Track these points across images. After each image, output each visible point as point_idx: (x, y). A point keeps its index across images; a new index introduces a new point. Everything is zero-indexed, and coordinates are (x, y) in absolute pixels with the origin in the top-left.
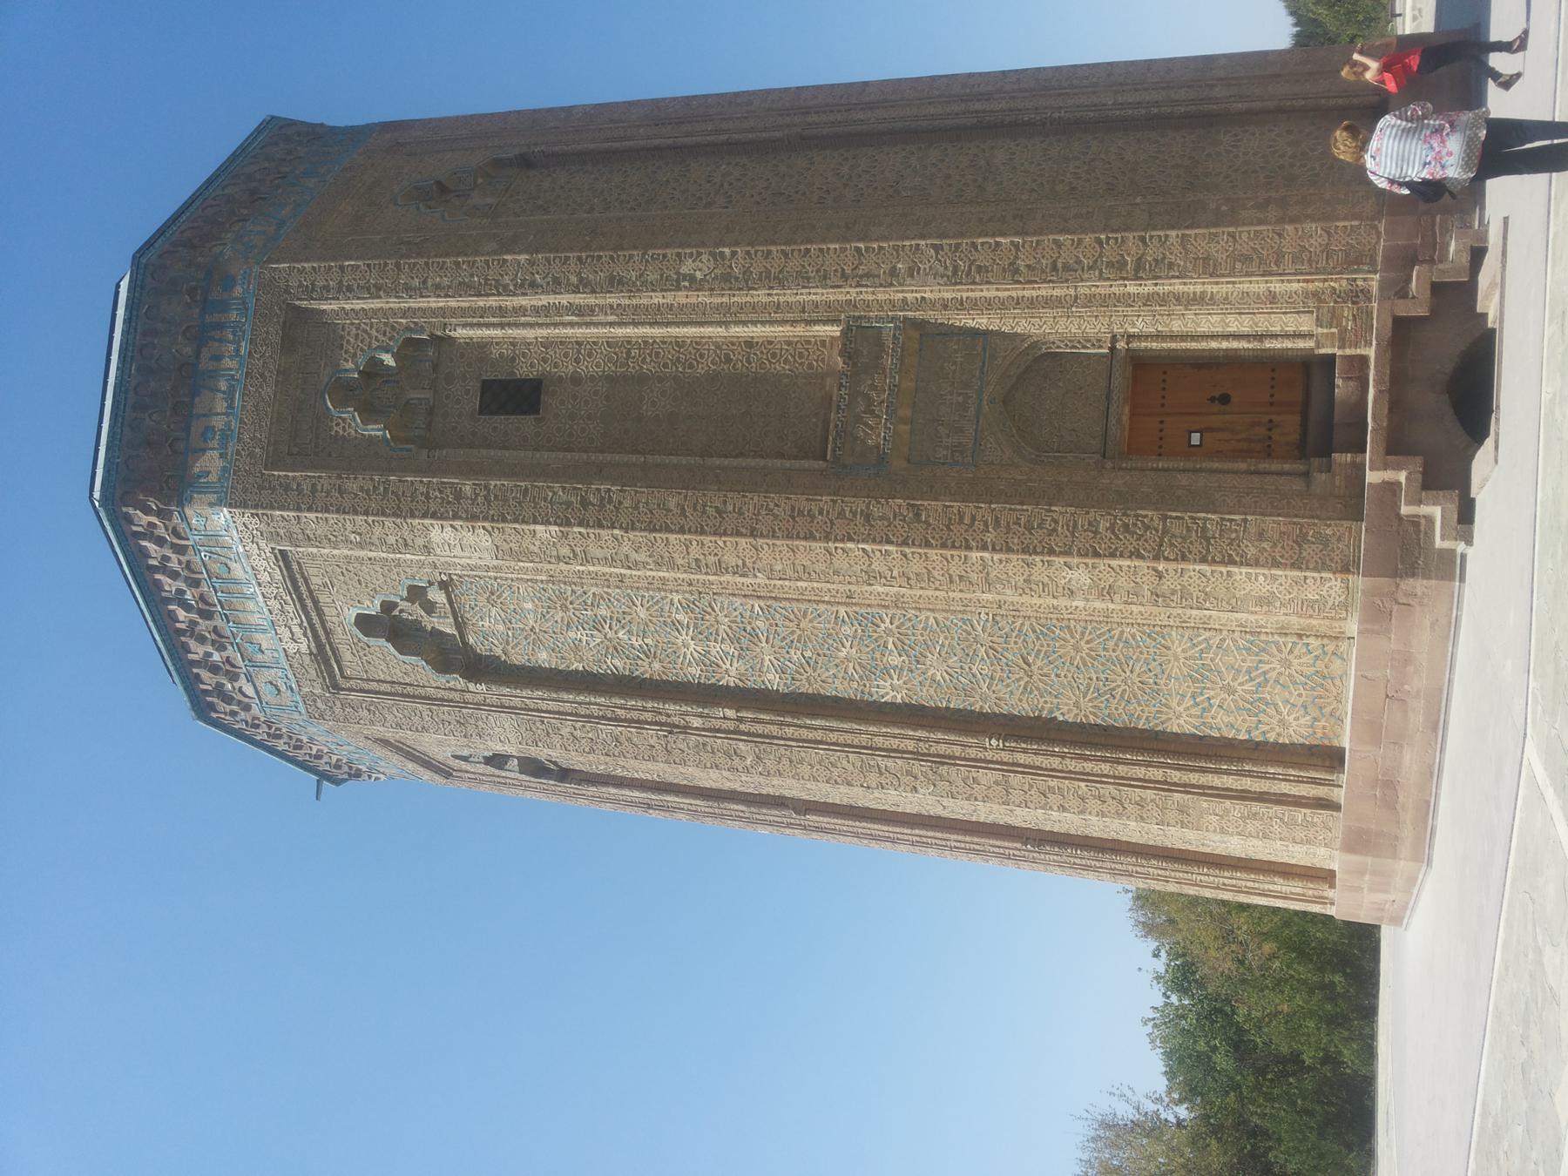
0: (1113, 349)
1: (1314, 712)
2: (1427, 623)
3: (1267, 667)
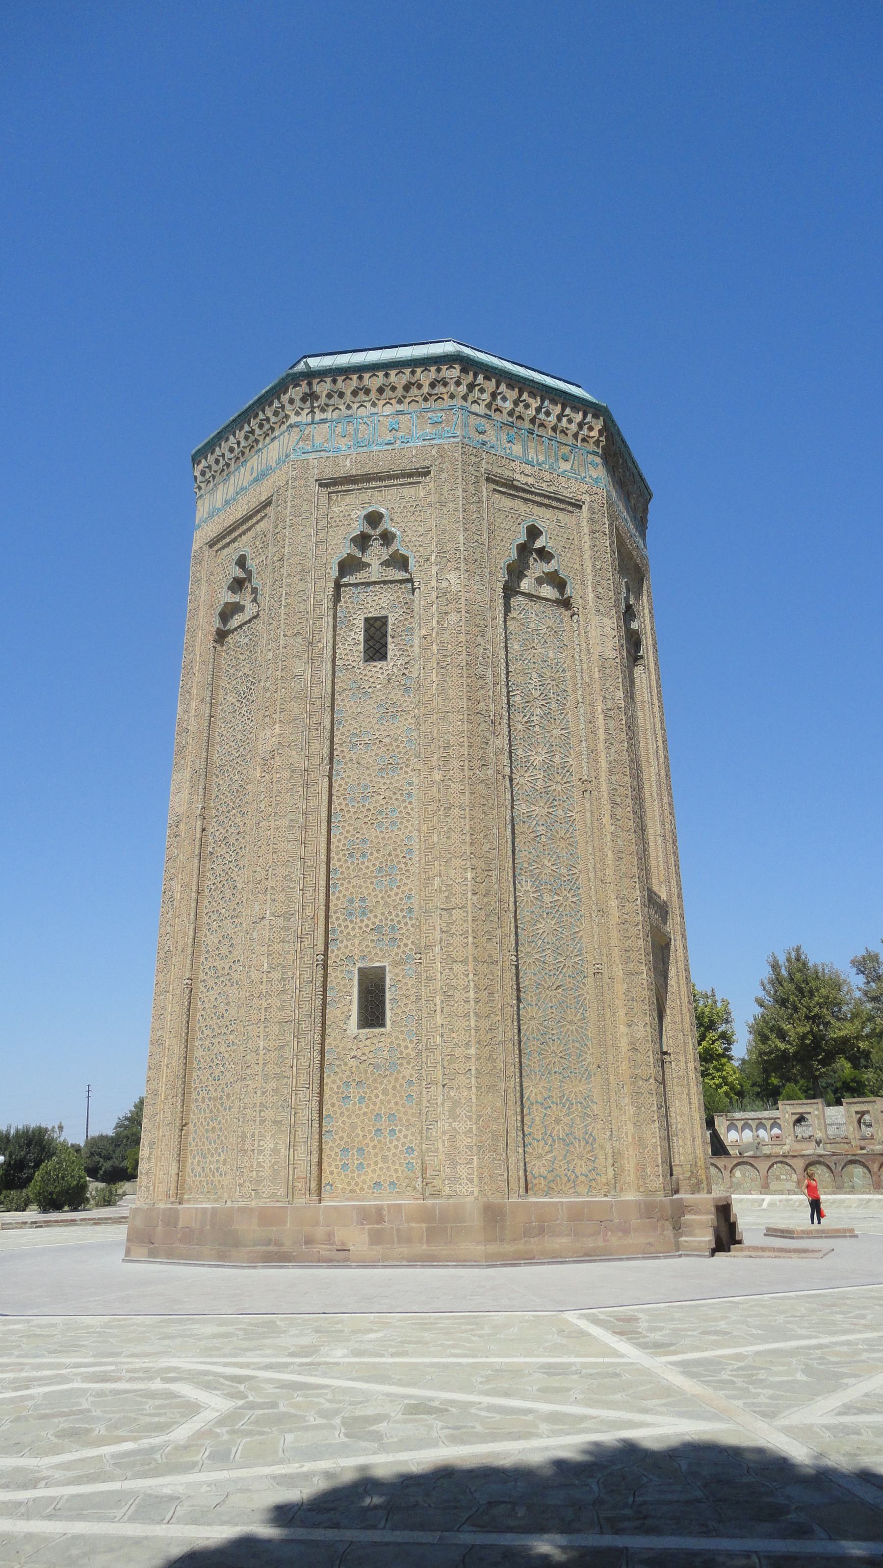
2: (651, 1240)
3: (577, 1145)
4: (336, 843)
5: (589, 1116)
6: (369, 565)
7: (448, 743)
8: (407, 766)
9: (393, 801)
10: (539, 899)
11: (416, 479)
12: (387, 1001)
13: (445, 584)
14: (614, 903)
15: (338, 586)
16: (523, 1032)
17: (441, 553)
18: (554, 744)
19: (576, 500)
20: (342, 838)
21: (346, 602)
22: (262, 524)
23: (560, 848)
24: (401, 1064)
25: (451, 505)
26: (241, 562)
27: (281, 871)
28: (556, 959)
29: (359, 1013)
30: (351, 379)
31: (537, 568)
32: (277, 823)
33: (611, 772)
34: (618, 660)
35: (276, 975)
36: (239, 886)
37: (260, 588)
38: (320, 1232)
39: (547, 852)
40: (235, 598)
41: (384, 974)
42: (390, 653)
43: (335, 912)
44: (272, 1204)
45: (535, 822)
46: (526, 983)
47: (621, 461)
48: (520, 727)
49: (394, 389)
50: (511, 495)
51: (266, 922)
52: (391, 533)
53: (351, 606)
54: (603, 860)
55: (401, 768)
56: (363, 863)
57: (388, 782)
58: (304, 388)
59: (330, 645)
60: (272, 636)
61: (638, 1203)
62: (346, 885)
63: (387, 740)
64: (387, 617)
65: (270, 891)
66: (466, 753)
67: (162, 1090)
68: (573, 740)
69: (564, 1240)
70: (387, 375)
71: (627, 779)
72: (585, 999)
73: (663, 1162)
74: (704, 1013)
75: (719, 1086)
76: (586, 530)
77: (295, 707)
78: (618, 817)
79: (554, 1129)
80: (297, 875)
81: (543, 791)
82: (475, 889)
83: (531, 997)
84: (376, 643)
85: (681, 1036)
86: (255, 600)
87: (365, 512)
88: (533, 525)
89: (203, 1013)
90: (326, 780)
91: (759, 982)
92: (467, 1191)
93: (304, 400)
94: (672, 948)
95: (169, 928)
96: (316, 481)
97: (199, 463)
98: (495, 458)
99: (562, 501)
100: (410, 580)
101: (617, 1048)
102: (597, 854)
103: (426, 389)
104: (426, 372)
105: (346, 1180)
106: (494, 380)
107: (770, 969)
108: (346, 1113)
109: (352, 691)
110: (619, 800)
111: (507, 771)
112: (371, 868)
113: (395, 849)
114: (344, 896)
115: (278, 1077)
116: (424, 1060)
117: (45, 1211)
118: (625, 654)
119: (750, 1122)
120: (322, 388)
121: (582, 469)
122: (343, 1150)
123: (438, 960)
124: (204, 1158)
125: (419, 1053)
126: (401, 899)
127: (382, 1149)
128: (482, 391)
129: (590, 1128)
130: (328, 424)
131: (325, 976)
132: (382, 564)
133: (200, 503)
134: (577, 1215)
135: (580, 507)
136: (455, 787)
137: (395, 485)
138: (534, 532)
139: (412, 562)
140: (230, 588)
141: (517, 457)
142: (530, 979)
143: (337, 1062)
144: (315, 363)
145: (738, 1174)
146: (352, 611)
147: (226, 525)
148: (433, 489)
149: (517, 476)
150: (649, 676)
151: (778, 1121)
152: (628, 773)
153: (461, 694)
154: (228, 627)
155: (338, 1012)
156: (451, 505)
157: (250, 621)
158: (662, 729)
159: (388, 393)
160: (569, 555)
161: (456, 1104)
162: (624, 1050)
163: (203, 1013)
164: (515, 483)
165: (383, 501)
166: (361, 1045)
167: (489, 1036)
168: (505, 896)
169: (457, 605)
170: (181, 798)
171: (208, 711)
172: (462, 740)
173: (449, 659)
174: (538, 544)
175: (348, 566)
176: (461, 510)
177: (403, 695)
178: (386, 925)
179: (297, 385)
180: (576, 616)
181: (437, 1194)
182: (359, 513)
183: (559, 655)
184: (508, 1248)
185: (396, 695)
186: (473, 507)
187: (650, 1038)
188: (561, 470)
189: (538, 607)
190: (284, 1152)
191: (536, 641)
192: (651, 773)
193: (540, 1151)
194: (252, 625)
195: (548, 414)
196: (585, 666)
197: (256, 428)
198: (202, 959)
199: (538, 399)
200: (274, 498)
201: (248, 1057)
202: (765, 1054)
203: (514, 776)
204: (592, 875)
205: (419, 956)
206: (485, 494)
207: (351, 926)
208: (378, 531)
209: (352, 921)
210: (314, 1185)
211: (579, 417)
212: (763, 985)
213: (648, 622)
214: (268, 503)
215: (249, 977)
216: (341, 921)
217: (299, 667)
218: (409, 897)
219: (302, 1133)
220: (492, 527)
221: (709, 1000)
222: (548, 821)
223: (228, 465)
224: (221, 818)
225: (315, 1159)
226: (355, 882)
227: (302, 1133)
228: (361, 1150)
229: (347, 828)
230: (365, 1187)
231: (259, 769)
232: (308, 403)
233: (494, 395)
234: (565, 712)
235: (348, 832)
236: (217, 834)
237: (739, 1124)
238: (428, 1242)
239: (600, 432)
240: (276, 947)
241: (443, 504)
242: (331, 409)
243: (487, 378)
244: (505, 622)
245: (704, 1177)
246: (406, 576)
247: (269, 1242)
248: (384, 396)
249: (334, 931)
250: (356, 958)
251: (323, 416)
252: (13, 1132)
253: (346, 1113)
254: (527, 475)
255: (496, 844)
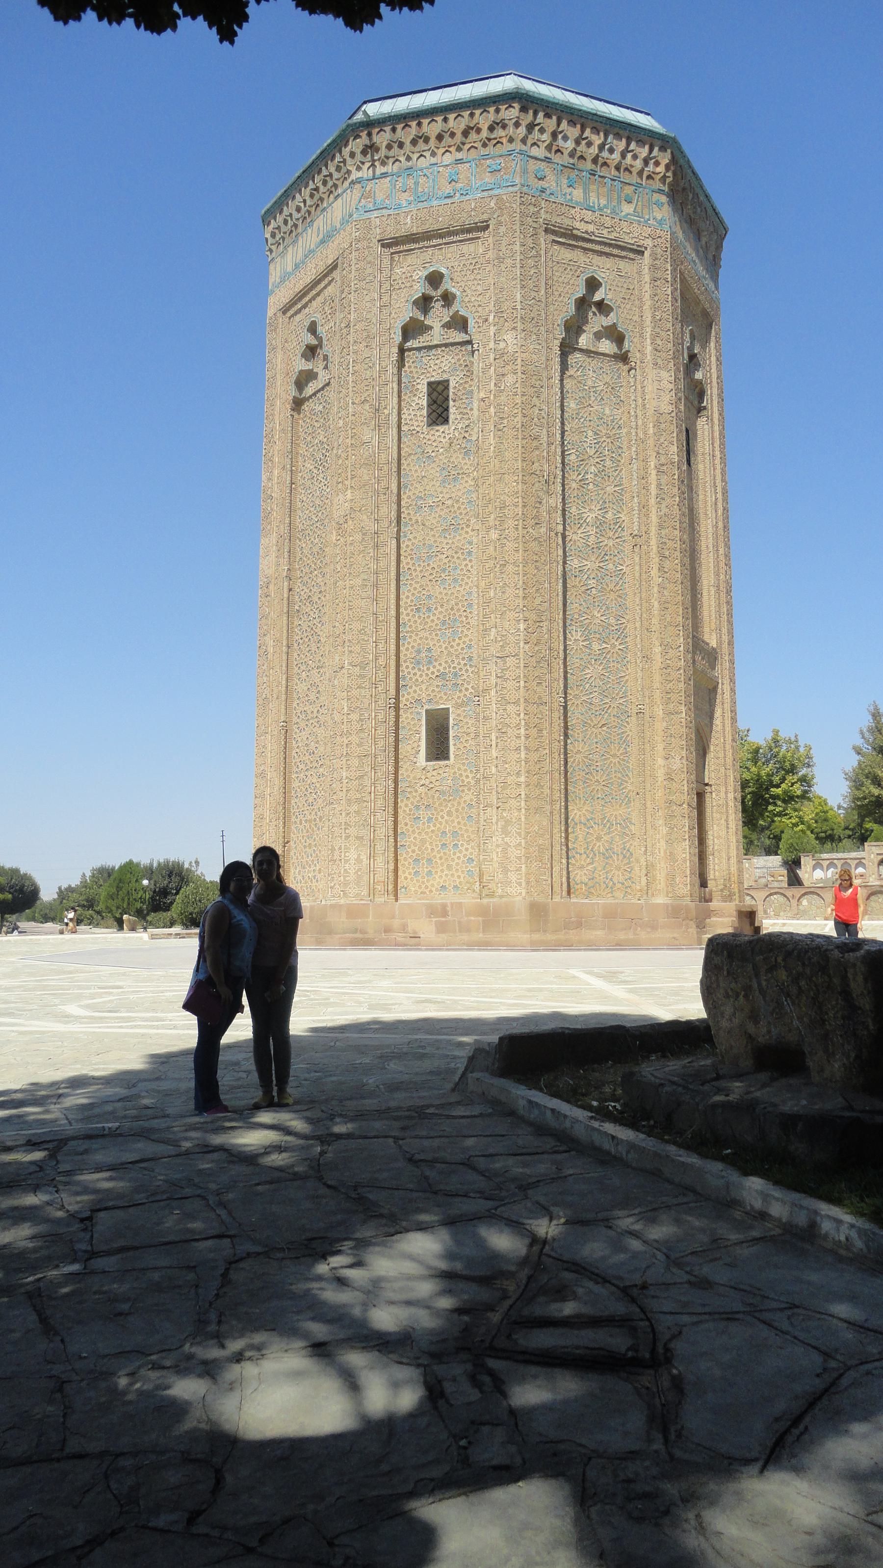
0: (707, 785)
1: (590, 884)
2: (675, 935)
4: (405, 600)
5: (627, 835)
6: (431, 328)
7: (504, 503)
8: (468, 526)
9: (455, 559)
11: (475, 235)
12: (451, 738)
13: (502, 345)
14: (658, 650)
15: (402, 351)
16: (569, 764)
17: (499, 312)
18: (607, 501)
19: (638, 246)
20: (410, 595)
21: (410, 367)
22: (329, 288)
23: (609, 600)
24: (463, 791)
25: (509, 261)
26: (313, 329)
27: (357, 626)
29: (427, 748)
30: (410, 126)
31: (596, 322)
32: (351, 582)
33: (661, 527)
34: (674, 414)
35: (355, 717)
36: (323, 640)
37: (330, 355)
38: (396, 923)
39: (597, 604)
40: (308, 366)
41: (448, 714)
42: (452, 417)
43: (405, 661)
44: (357, 902)
45: (586, 576)
46: (574, 722)
47: (691, 196)
48: (574, 485)
49: (453, 135)
50: (570, 245)
51: (344, 671)
52: (452, 294)
53: (414, 370)
54: (649, 610)
55: (462, 528)
56: (429, 617)
57: (450, 542)
58: (364, 140)
59: (395, 411)
60: (342, 404)
61: (666, 906)
62: (414, 637)
63: (449, 502)
64: (448, 381)
65: (347, 644)
66: (520, 513)
67: (267, 814)
68: (626, 497)
69: (600, 933)
70: (445, 120)
71: (677, 532)
72: (628, 736)
73: (691, 874)
74: (785, 758)
75: (796, 825)
76: (647, 278)
77: (365, 474)
78: (666, 570)
79: (595, 844)
80: (370, 629)
81: (595, 546)
82: (527, 638)
84: (439, 409)
85: (723, 770)
86: (326, 367)
87: (426, 273)
88: (593, 277)
89: (298, 750)
90: (394, 541)
91: (858, 730)
92: (516, 892)
93: (364, 152)
94: (719, 691)
95: (265, 679)
96: (379, 241)
97: (269, 224)
98: (554, 205)
99: (622, 248)
100: (470, 342)
101: (654, 777)
102: (644, 604)
103: (485, 133)
104: (485, 114)
105: (418, 884)
106: (554, 118)
107: (870, 718)
108: (417, 831)
109: (417, 456)
110: (667, 553)
111: (560, 528)
112: (436, 621)
113: (457, 604)
114: (413, 647)
115: (359, 801)
116: (482, 787)
117: (187, 928)
118: (682, 408)
119: (835, 861)
120: (382, 138)
121: (646, 211)
122: (416, 860)
123: (494, 702)
124: (304, 868)
125: (478, 781)
126: (462, 649)
127: (447, 859)
128: (542, 131)
129: (628, 845)
130: (388, 179)
131: (397, 717)
132: (443, 326)
133: (272, 267)
134: (611, 915)
135: (642, 253)
136: (510, 545)
137: (455, 242)
138: (593, 284)
139: (471, 323)
140: (304, 355)
141: (577, 203)
142: (578, 719)
143: (409, 790)
144: (374, 110)
145: (805, 902)
146: (416, 376)
147: (297, 290)
148: (492, 245)
149: (577, 225)
150: (712, 427)
151: (863, 861)
152: (678, 527)
153: (516, 455)
154: (303, 395)
155: (409, 748)
156: (509, 261)
157: (323, 389)
158: (723, 481)
159: (447, 140)
160: (628, 307)
161: (508, 822)
162: (660, 779)
163: (298, 750)
164: (575, 232)
165: (445, 259)
166: (429, 775)
167: (538, 766)
168: (555, 645)
169: (513, 366)
170: (269, 562)
171: (289, 478)
172: (516, 500)
173: (505, 421)
174: (597, 297)
175: (411, 330)
176: (518, 266)
177: (464, 458)
178: (450, 672)
179: (357, 136)
180: (633, 371)
181: (491, 895)
182: (420, 273)
183: (615, 412)
184: (550, 937)
185: (458, 458)
186: (531, 262)
187: (685, 770)
188: (623, 213)
189: (595, 363)
190: (365, 861)
191: (593, 399)
192: (707, 527)
193: (582, 863)
194: (324, 392)
195: (611, 151)
196: (640, 422)
197: (320, 184)
198: (295, 705)
199: (602, 134)
200: (340, 261)
201: (334, 785)
202: (858, 799)
203: (567, 533)
204: (638, 624)
205: (478, 698)
206: (543, 246)
207: (419, 673)
208: (440, 292)
209: (419, 669)
210: (391, 887)
211: (644, 152)
212: (862, 733)
213: (714, 370)
214: (334, 267)
215: (333, 719)
216: (409, 670)
217: (367, 434)
218: (470, 647)
219: (380, 847)
220: (550, 282)
221: (792, 746)
222: (599, 575)
223: (296, 226)
224: (305, 579)
225: (392, 866)
226: (421, 634)
227: (380, 847)
228: (429, 860)
229: (415, 585)
230: (434, 889)
231: (334, 533)
232: (369, 156)
233: (554, 135)
234: (619, 468)
235: (415, 589)
236: (302, 593)
237: (825, 864)
238: (483, 932)
239: (667, 167)
240: (355, 692)
241: (501, 260)
242: (391, 161)
243: (548, 116)
244: (562, 380)
245: (737, 890)
246: (466, 338)
247: (356, 931)
248: (443, 143)
249: (404, 678)
250: (424, 701)
251: (384, 170)
252: (155, 865)
253: (417, 831)
254: (587, 222)
255: (547, 597)
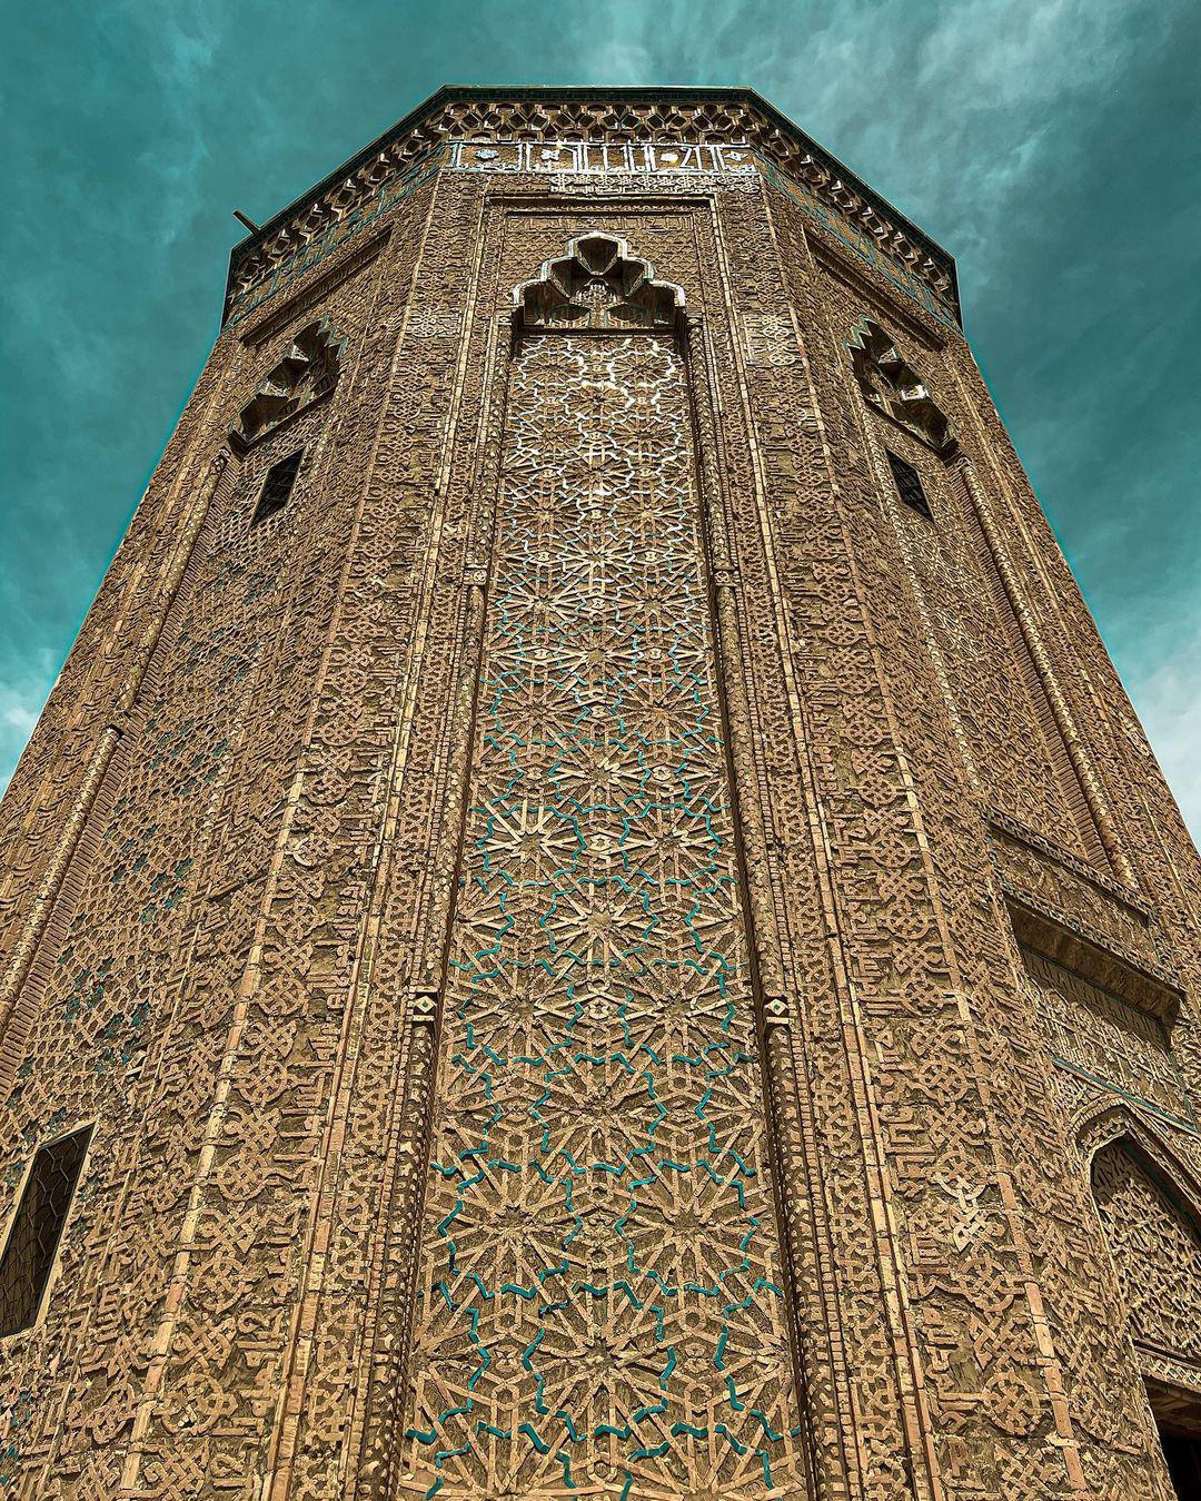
10: (579, 850)
28: (625, 1010)
83: (517, 1140)
